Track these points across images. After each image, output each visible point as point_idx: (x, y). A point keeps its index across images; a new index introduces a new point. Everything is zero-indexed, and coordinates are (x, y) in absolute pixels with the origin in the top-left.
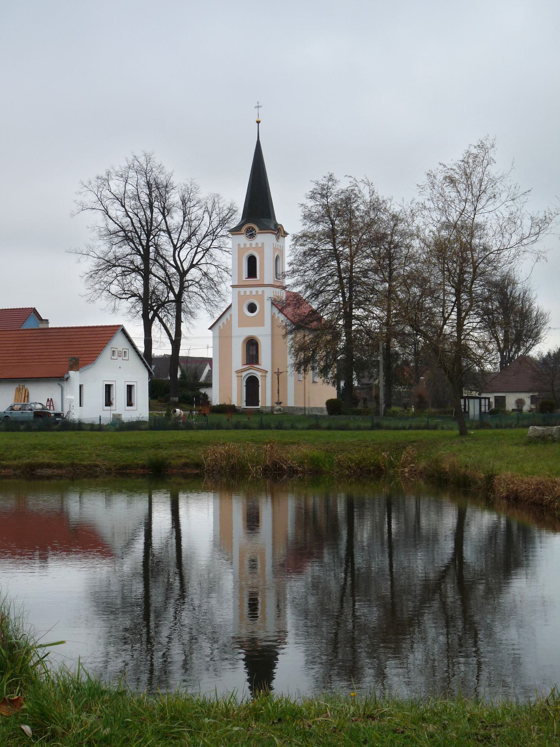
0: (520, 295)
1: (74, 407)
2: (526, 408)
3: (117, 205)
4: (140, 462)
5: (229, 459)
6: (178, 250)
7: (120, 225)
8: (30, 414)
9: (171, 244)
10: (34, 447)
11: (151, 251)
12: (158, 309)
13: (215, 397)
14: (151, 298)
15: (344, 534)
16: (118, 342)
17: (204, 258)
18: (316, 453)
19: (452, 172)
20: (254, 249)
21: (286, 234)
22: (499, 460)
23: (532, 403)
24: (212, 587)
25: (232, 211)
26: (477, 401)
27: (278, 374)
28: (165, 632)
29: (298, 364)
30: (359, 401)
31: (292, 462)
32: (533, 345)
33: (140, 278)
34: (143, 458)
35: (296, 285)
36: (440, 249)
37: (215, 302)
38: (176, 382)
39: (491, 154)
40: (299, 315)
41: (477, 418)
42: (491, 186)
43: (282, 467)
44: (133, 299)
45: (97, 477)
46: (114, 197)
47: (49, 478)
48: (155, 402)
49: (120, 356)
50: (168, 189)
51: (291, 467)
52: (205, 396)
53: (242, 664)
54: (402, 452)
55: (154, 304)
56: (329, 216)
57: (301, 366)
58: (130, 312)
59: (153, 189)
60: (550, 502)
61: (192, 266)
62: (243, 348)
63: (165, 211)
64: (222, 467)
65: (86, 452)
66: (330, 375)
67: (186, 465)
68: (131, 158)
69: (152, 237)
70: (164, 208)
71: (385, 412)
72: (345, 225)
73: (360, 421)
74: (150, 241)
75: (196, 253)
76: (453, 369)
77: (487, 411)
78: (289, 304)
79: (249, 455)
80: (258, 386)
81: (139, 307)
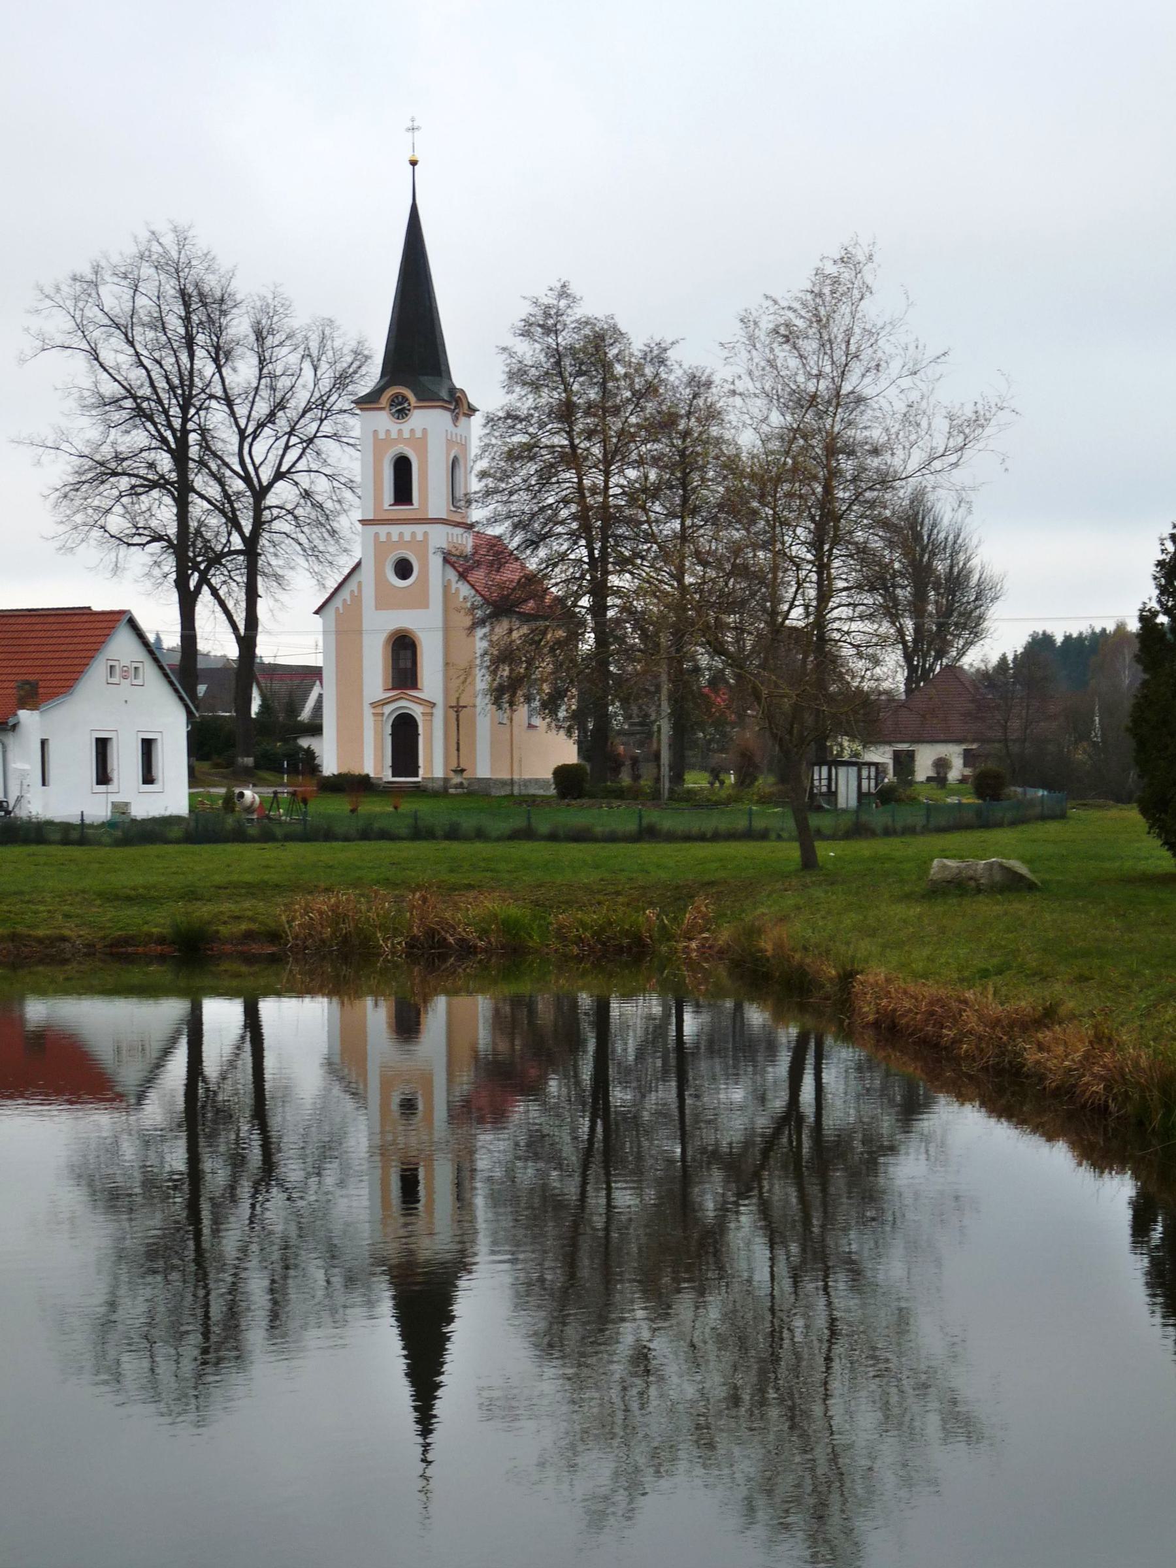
0: (946, 539)
1: (31, 789)
2: (954, 775)
3: (118, 341)
4: (154, 930)
5: (337, 924)
6: (249, 440)
7: (125, 383)
9: (236, 429)
11: (191, 442)
12: (208, 569)
14: (194, 545)
16: (122, 647)
17: (304, 460)
18: (514, 911)
19: (791, 315)
20: (407, 441)
21: (472, 410)
22: (869, 936)
23: (965, 765)
24: (328, 1150)
25: (361, 357)
26: (853, 770)
27: (457, 710)
28: (230, 1243)
29: (496, 690)
30: (623, 764)
31: (464, 930)
32: (972, 643)
33: (168, 500)
34: (159, 921)
35: (494, 520)
37: (327, 555)
38: (245, 722)
40: (501, 586)
41: (853, 803)
42: (869, 343)
43: (445, 939)
44: (156, 546)
45: (65, 961)
46: (110, 323)
48: (205, 766)
49: (125, 678)
50: (224, 307)
51: (463, 940)
52: (310, 754)
53: (386, 1307)
54: (686, 906)
55: (199, 559)
56: (561, 374)
58: (148, 575)
59: (194, 306)
60: (954, 1041)
61: (279, 476)
62: (385, 659)
63: (220, 355)
64: (323, 941)
65: (42, 908)
66: (562, 714)
67: (249, 936)
68: (144, 235)
69: (192, 411)
70: (218, 348)
71: (671, 791)
72: (593, 394)
74: (190, 420)
75: (287, 447)
76: (809, 707)
77: (873, 790)
78: (479, 561)
79: (378, 916)
80: (416, 735)
81: (169, 564)
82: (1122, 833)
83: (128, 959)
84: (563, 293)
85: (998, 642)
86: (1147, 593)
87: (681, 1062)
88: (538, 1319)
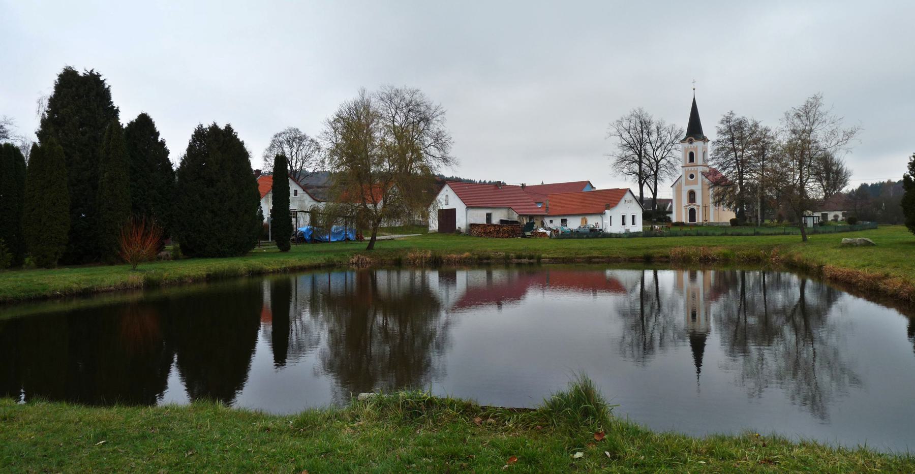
2: (839, 219)
3: (626, 132)
8: (588, 230)
10: (591, 249)
13: (674, 218)
15: (740, 283)
16: (628, 196)
18: (726, 251)
24: (673, 306)
25: (681, 131)
27: (705, 207)
28: (651, 324)
34: (641, 253)
36: (791, 149)
38: (655, 212)
39: (821, 101)
47: (598, 263)
57: (717, 203)
63: (649, 134)
67: (661, 257)
73: (750, 230)
81: (637, 178)
82: (901, 232)
83: (633, 262)
84: (731, 113)
85: (852, 185)
86: (907, 171)
87: (765, 289)
88: (728, 348)
